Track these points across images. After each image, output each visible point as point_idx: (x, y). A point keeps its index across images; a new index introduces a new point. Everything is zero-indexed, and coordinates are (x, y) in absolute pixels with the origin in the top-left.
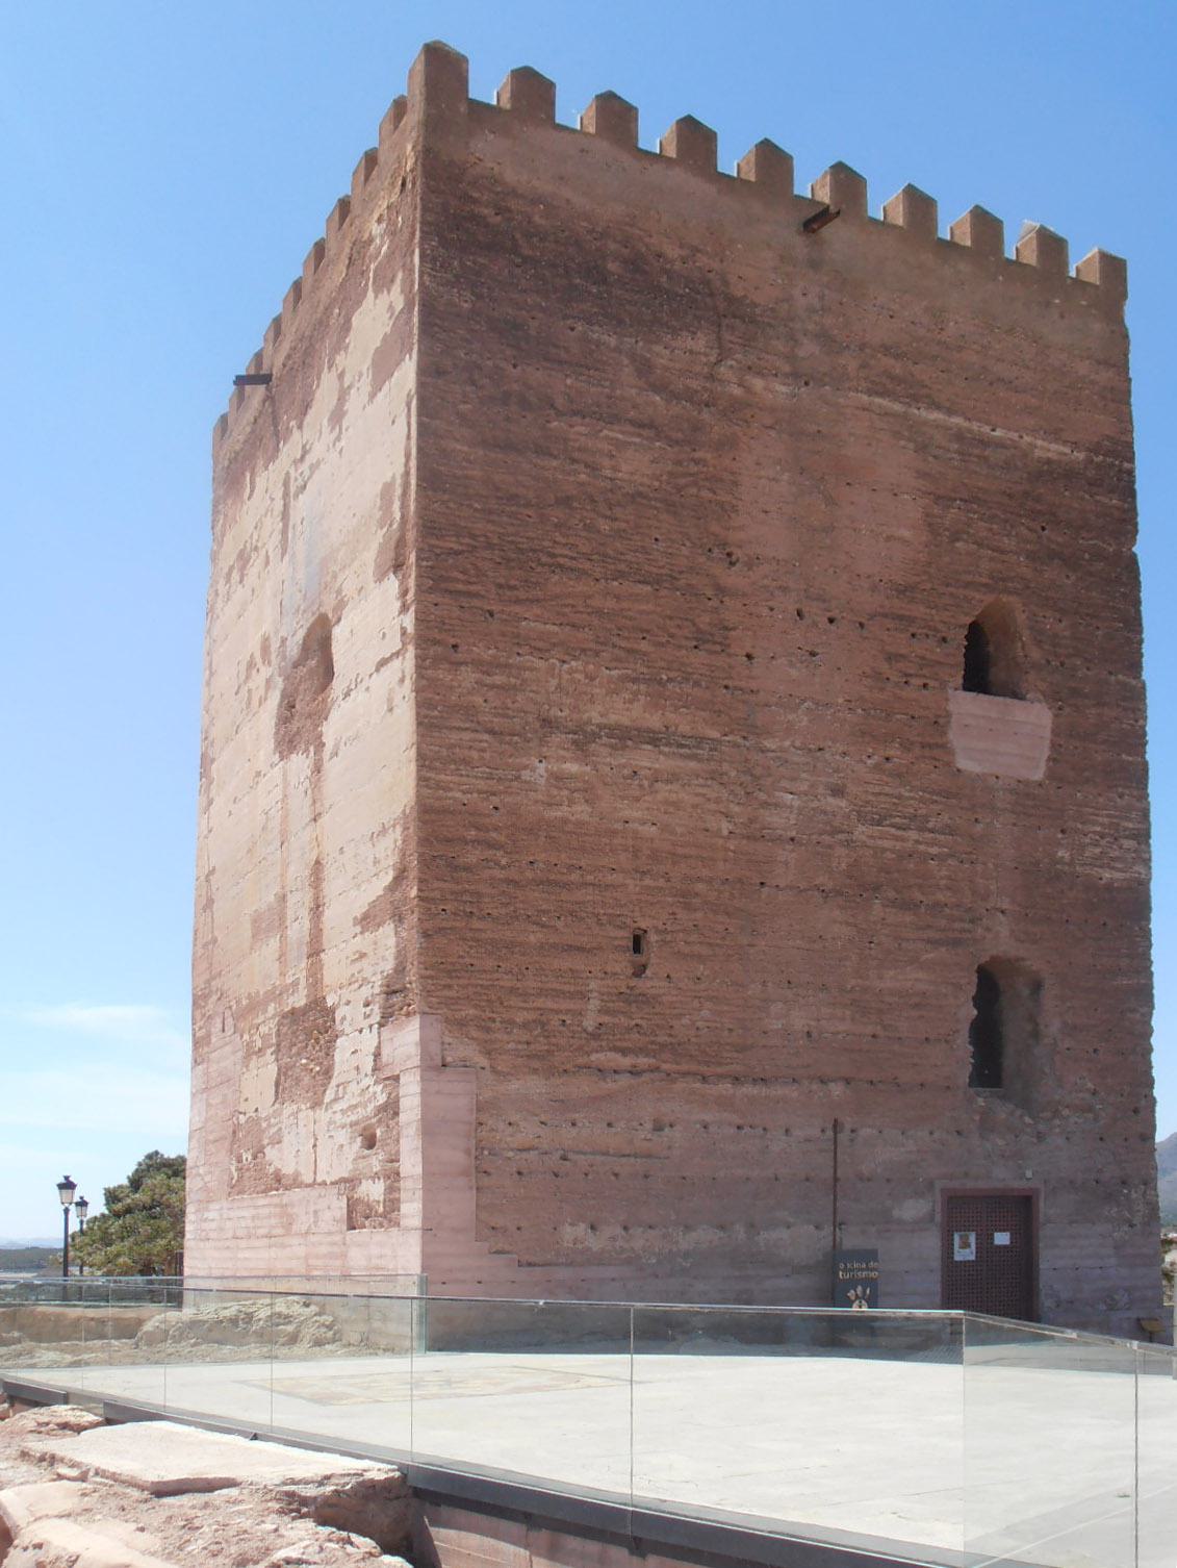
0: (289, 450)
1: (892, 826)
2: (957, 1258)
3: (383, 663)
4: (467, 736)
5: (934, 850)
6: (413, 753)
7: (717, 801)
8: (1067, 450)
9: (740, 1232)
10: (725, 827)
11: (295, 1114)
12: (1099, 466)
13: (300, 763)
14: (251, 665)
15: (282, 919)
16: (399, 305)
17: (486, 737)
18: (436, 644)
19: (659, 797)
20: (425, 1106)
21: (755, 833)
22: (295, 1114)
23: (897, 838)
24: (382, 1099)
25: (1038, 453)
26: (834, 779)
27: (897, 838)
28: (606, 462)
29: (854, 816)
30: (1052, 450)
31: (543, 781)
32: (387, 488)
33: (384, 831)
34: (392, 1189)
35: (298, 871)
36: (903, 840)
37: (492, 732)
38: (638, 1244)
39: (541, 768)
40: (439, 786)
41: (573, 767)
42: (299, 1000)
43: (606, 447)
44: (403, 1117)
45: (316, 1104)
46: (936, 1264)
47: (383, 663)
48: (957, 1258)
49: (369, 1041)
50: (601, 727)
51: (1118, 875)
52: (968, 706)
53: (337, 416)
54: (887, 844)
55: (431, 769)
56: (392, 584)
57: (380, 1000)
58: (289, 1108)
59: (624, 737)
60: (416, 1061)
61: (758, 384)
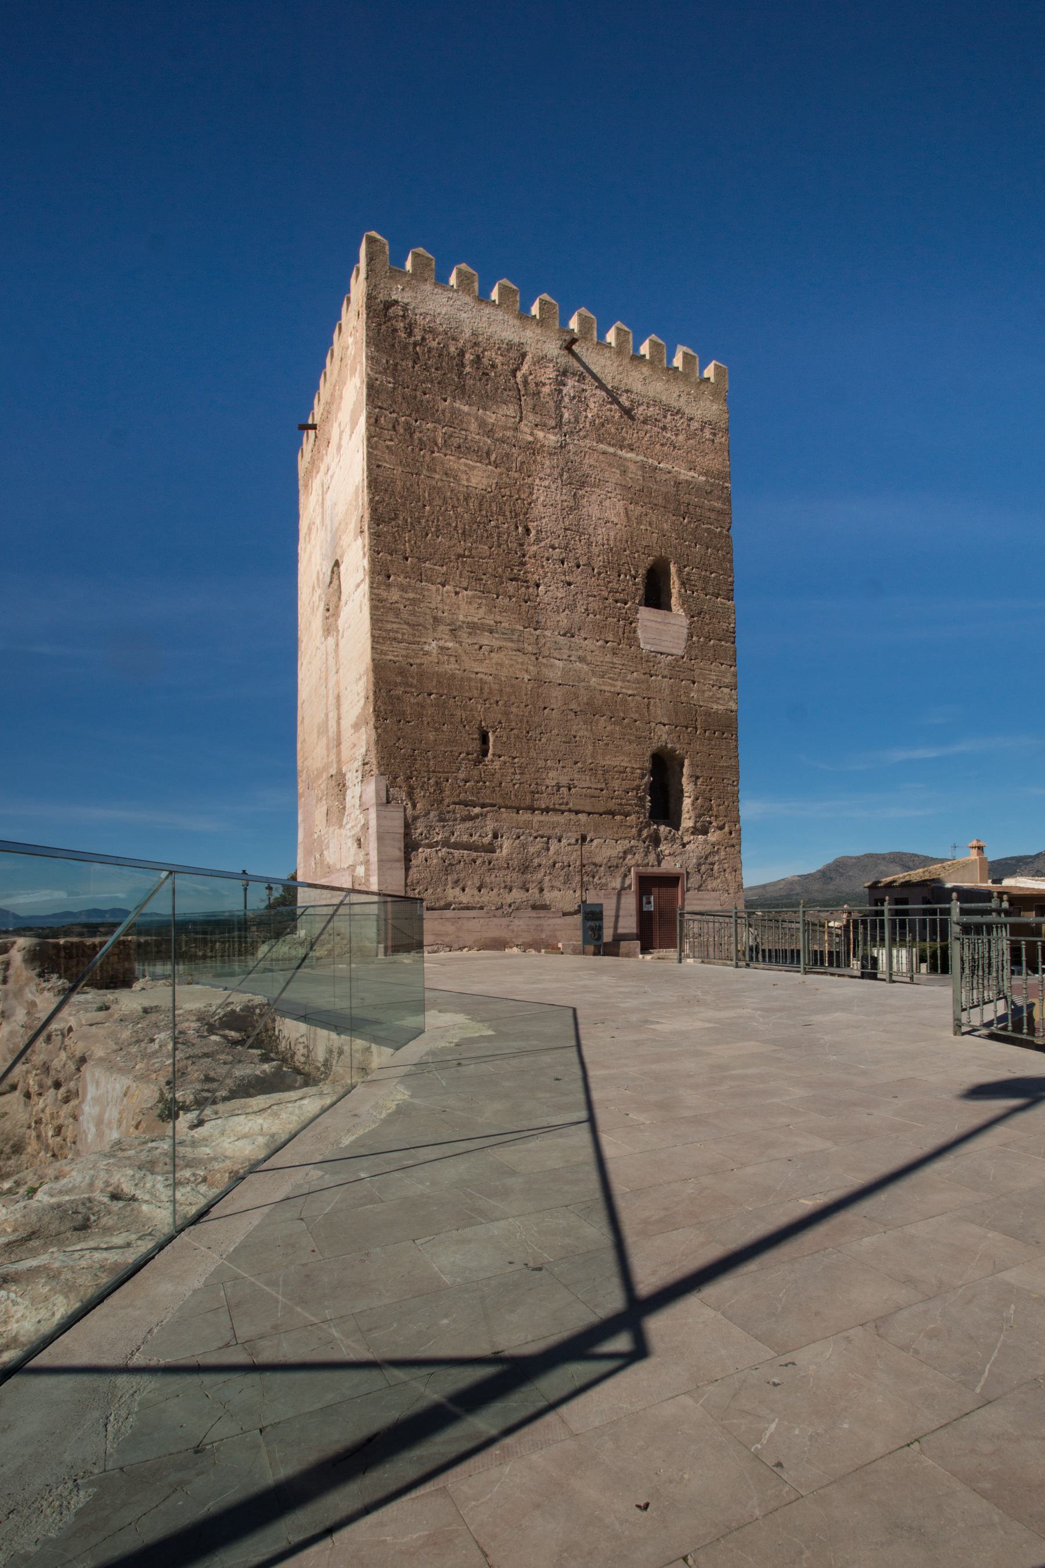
0: (323, 468)
1: (610, 678)
2: (645, 909)
3: (358, 586)
4: (395, 626)
5: (630, 692)
6: (369, 634)
7: (522, 663)
8: (696, 475)
9: (534, 891)
10: (527, 677)
11: (333, 832)
12: (712, 485)
13: (331, 640)
14: (314, 587)
15: (327, 727)
16: (358, 385)
17: (406, 627)
18: (380, 573)
19: (494, 661)
20: (379, 826)
21: (540, 681)
22: (333, 832)
23: (611, 685)
24: (363, 822)
25: (682, 477)
26: (580, 653)
27: (611, 685)
28: (465, 477)
29: (590, 673)
30: (686, 474)
31: (435, 651)
32: (357, 487)
33: (360, 678)
34: (367, 870)
35: (332, 700)
36: (615, 686)
37: (408, 624)
38: (485, 899)
39: (434, 644)
40: (382, 653)
41: (450, 645)
42: (333, 771)
43: (463, 468)
44: (370, 830)
45: (341, 826)
46: (634, 913)
47: (358, 586)
48: (645, 909)
49: (358, 790)
50: (463, 622)
51: (720, 707)
52: (646, 614)
53: (339, 447)
54: (607, 688)
55: (378, 643)
56: (360, 541)
57: (361, 769)
58: (331, 829)
59: (474, 628)
60: (374, 801)
61: (540, 434)
